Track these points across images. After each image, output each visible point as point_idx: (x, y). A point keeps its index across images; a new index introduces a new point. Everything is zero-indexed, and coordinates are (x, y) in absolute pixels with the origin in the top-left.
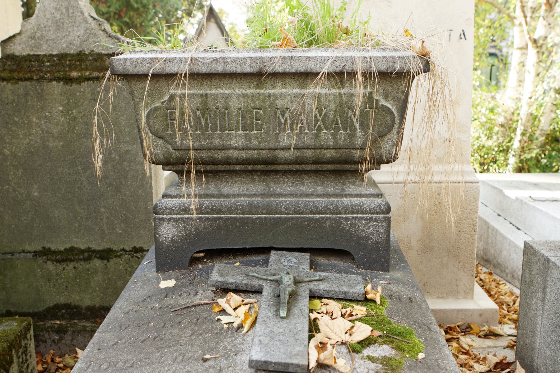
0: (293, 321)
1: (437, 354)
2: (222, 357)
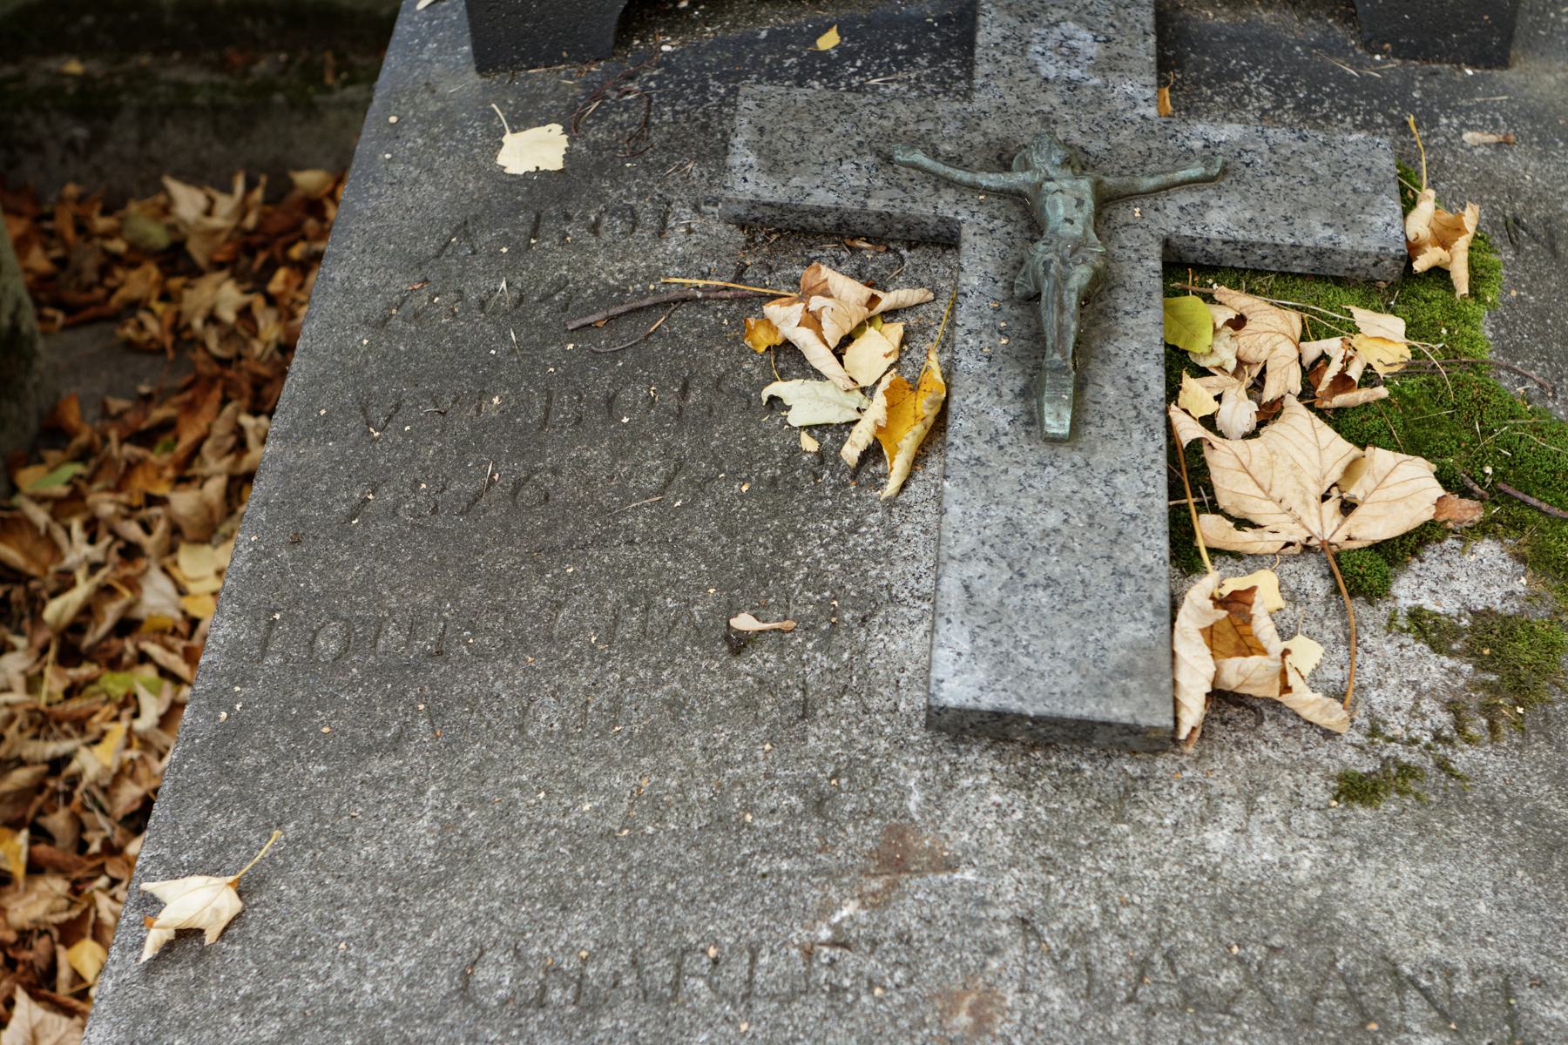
0: (1103, 458)
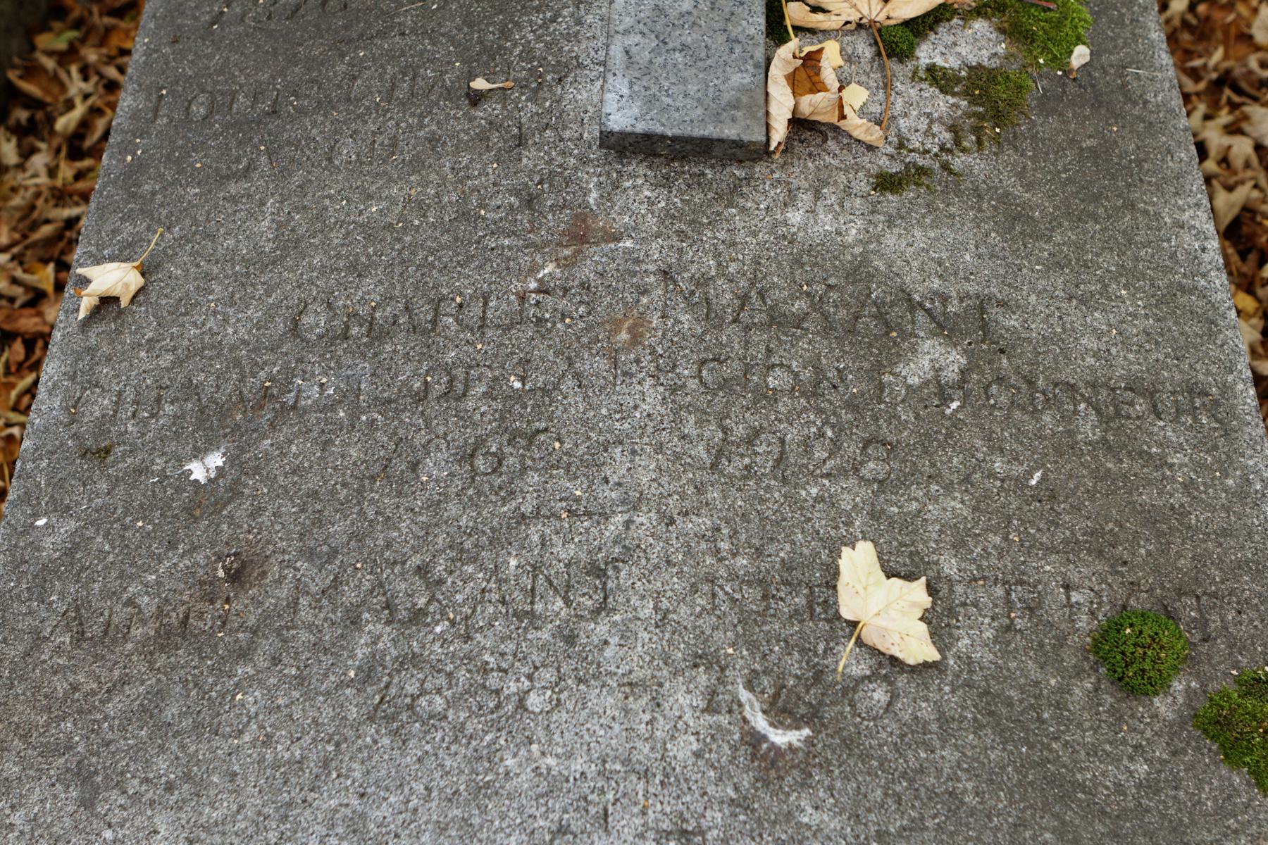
1: (1126, 45)
2: (523, 86)
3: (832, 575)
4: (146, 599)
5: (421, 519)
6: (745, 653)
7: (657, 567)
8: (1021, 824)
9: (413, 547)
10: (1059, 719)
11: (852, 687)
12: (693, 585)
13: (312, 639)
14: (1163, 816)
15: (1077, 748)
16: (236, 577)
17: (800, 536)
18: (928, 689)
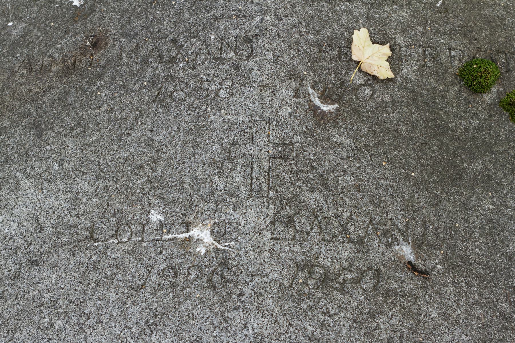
3: (350, 41)
4: (57, 55)
5: (174, 20)
6: (311, 74)
7: (274, 38)
8: (425, 143)
9: (170, 31)
10: (443, 102)
11: (357, 88)
12: (289, 46)
13: (128, 70)
14: (484, 141)
15: (450, 114)
16: (95, 45)
17: (336, 26)
18: (388, 89)
